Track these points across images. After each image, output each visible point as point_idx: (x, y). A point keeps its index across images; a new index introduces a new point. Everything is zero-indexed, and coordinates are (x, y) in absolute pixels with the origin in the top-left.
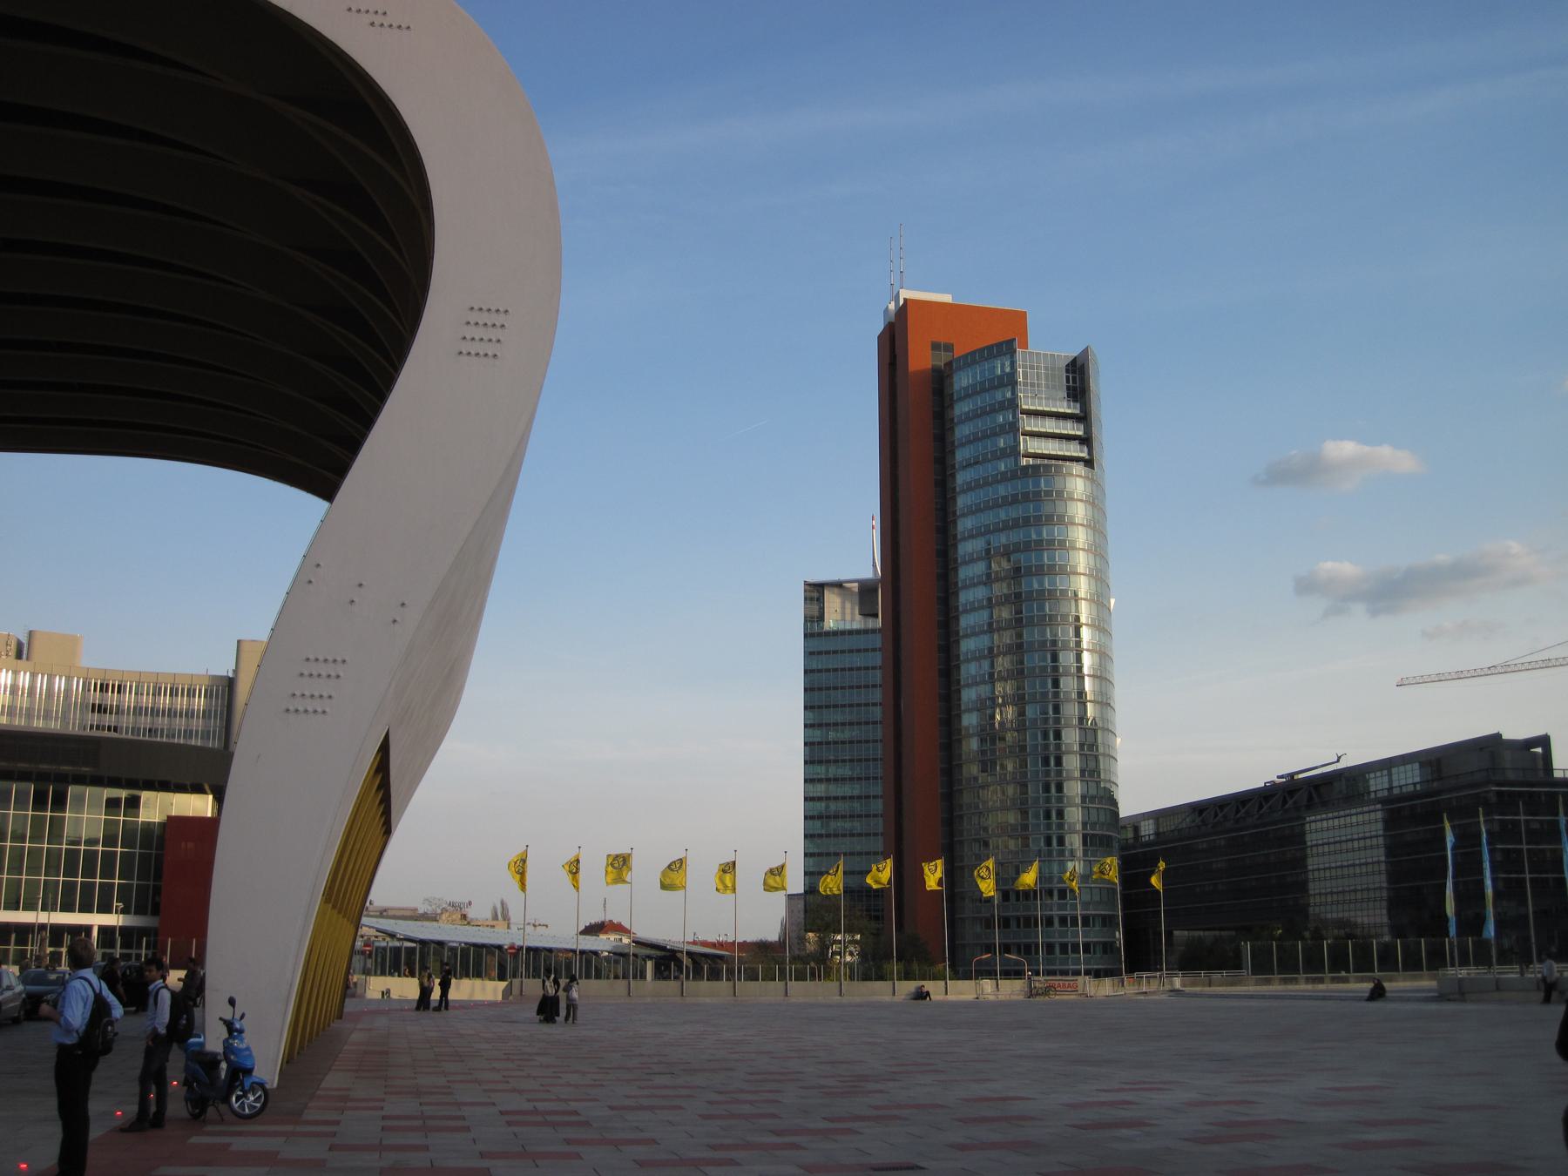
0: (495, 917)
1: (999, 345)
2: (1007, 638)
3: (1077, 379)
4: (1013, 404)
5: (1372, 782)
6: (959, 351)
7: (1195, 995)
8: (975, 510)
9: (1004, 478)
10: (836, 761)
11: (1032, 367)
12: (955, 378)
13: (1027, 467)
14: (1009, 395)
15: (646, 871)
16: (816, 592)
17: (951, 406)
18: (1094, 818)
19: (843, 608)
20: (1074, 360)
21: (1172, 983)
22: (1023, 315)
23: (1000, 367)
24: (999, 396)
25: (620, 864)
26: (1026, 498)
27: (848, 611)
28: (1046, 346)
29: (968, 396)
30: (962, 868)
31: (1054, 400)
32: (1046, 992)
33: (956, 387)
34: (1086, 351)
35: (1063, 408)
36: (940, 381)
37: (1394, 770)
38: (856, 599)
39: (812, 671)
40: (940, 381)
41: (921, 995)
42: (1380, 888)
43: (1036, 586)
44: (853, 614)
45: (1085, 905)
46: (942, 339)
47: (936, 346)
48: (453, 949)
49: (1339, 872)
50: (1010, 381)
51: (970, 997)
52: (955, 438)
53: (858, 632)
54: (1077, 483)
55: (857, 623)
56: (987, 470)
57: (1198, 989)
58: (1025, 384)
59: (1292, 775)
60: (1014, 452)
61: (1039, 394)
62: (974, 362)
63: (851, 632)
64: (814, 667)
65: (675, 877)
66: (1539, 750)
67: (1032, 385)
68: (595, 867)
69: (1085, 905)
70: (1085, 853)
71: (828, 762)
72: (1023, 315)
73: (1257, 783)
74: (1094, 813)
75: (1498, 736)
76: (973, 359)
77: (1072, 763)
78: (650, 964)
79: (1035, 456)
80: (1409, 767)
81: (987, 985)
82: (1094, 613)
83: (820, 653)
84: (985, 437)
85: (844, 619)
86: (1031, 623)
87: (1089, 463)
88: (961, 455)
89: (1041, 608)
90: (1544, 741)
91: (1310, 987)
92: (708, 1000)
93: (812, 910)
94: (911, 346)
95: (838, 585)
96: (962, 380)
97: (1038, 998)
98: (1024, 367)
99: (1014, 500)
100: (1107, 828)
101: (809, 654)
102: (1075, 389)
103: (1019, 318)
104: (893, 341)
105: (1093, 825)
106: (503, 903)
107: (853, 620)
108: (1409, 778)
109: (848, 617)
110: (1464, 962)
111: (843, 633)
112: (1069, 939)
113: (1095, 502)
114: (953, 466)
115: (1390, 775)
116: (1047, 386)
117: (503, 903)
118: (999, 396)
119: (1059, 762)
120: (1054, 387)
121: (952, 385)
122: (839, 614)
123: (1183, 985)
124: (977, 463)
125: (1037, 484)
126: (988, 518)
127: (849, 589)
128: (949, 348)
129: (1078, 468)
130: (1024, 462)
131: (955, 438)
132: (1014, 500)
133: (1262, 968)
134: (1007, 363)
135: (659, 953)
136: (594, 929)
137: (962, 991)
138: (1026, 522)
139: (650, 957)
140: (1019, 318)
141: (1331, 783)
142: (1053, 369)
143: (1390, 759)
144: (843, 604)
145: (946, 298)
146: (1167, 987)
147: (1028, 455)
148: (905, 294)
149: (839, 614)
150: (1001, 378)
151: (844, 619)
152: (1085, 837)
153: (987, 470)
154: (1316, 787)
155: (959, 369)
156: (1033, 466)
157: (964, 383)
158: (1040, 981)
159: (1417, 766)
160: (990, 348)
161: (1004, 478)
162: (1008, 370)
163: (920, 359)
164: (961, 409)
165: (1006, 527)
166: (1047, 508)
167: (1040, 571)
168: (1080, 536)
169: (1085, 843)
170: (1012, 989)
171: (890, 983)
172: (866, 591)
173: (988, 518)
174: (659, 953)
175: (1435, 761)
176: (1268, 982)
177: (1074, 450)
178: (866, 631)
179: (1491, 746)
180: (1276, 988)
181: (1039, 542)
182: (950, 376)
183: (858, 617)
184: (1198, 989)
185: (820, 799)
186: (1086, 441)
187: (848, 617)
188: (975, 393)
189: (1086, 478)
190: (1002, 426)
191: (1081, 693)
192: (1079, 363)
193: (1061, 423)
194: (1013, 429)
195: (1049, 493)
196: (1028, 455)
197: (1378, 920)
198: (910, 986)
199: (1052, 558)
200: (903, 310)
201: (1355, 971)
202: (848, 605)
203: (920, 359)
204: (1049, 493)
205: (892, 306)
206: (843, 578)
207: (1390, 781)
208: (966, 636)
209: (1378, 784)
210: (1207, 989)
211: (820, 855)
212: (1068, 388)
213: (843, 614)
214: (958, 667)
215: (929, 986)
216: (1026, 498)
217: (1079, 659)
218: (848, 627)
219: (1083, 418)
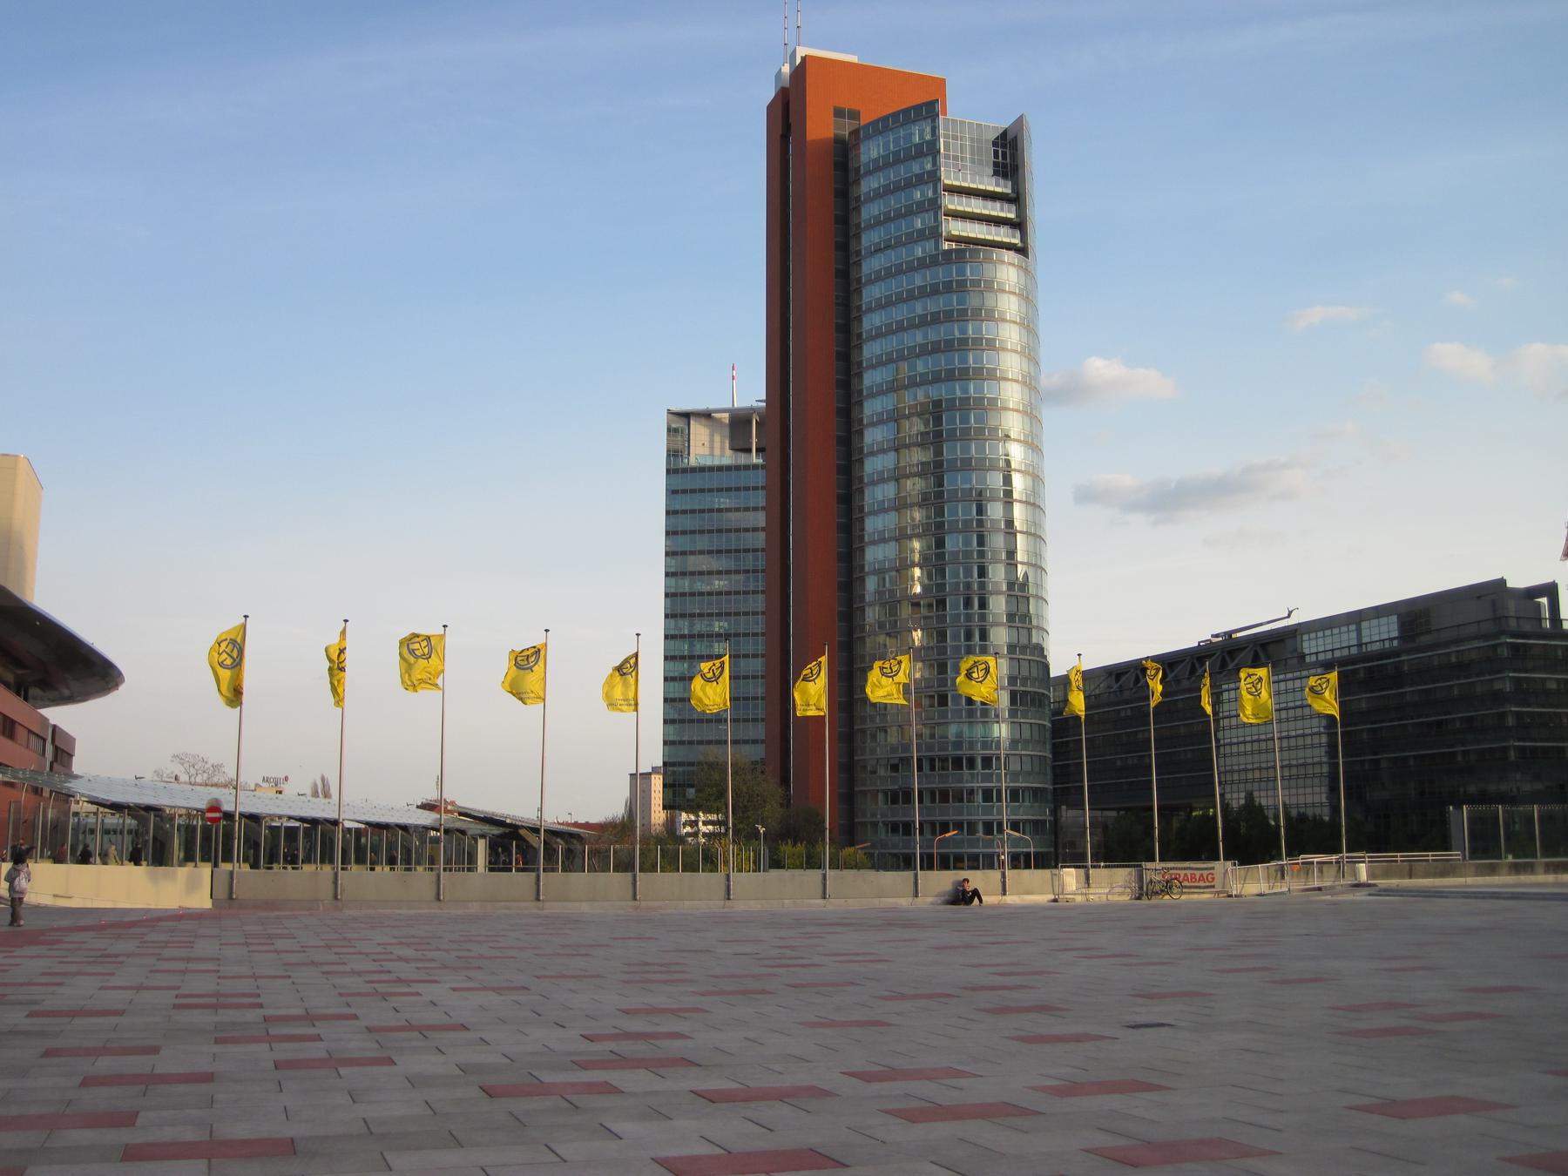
0: (315, 794)
1: (918, 108)
2: (917, 456)
3: (1008, 154)
4: (934, 177)
5: (1305, 644)
6: (865, 119)
7: (1387, 891)
8: (886, 304)
9: (922, 264)
10: (701, 615)
11: (955, 138)
12: (863, 148)
13: (950, 251)
14: (929, 167)
15: (475, 664)
16: (683, 418)
17: (857, 182)
18: (1025, 672)
19: (712, 441)
20: (1004, 134)
21: (1355, 874)
22: (942, 82)
23: (918, 133)
24: (916, 168)
25: (419, 655)
26: (948, 288)
27: (717, 445)
28: (972, 111)
29: (878, 169)
30: (863, 731)
31: (981, 176)
32: (1167, 888)
33: (864, 159)
34: (1020, 121)
35: (991, 185)
36: (843, 155)
37: (1365, 624)
38: (727, 431)
39: (676, 512)
40: (843, 155)
41: (963, 897)
42: (1321, 763)
43: (958, 393)
44: (722, 449)
45: (1014, 776)
46: (847, 105)
47: (839, 113)
48: (274, 830)
49: (1300, 741)
50: (930, 149)
51: (1044, 898)
52: (862, 228)
53: (729, 468)
54: (1007, 271)
55: (729, 458)
56: (900, 256)
57: (1394, 882)
58: (947, 157)
59: (1229, 634)
60: (935, 233)
61: (964, 168)
62: (886, 129)
63: (720, 468)
64: (678, 507)
65: (531, 680)
66: (1544, 600)
67: (956, 158)
68: (372, 662)
69: (1014, 776)
70: (1013, 713)
71: (692, 615)
72: (942, 82)
73: (595, 819)
74: (1025, 665)
75: (1502, 582)
76: (883, 125)
77: (999, 605)
78: (482, 845)
79: (959, 240)
80: (1384, 620)
81: (1070, 877)
82: (1028, 427)
83: (684, 492)
84: (899, 216)
85: (712, 454)
86: (952, 436)
87: (1022, 250)
88: (869, 239)
89: (965, 420)
90: (1551, 590)
91: (1551, 878)
92: (585, 907)
93: (686, 780)
94: (811, 111)
95: (706, 415)
96: (871, 151)
97: (1155, 900)
98: (946, 136)
99: (934, 291)
100: (1034, 688)
101: (672, 492)
102: (1004, 165)
103: (941, 83)
104: (786, 113)
105: (1024, 681)
106: (323, 779)
107: (722, 455)
108: (1384, 633)
109: (717, 452)
110: (1054, 851)
111: (711, 469)
112: (994, 817)
113: (1027, 297)
114: (858, 253)
115: (1359, 631)
116: (973, 161)
117: (323, 779)
118: (916, 168)
119: (983, 604)
120: (980, 162)
121: (858, 156)
122: (706, 448)
123: (1371, 875)
124: (888, 247)
125: (962, 272)
126: (899, 313)
127: (719, 421)
128: (854, 115)
129: (1009, 256)
130: (946, 246)
131: (862, 228)
132: (934, 291)
133: (1484, 847)
134: (928, 129)
135: (496, 831)
136: (428, 807)
137: (1030, 890)
138: (948, 317)
139: (483, 836)
140: (941, 83)
141: (1282, 641)
142: (979, 141)
143: (1360, 612)
144: (712, 436)
145: (854, 59)
146: (1349, 881)
147: (950, 239)
148: (802, 52)
149: (706, 448)
150: (919, 147)
151: (712, 454)
152: (1013, 695)
153: (900, 256)
154: (1264, 646)
155: (868, 137)
156: (956, 250)
157: (874, 154)
158: (1155, 869)
159: (1394, 618)
160: (906, 111)
161: (922, 264)
162: (928, 137)
163: (820, 126)
164: (869, 185)
165: (923, 322)
166: (973, 301)
167: (964, 375)
168: (1010, 335)
169: (1013, 700)
170: (1108, 886)
171: (909, 874)
172: (739, 423)
173: (899, 313)
174: (496, 831)
175: (1415, 616)
176: (1493, 870)
177: (1002, 235)
178: (738, 468)
179: (1495, 590)
180: (1503, 880)
181: (964, 341)
182: (857, 146)
183: (728, 452)
184: (1394, 882)
185: (683, 658)
186: (1019, 225)
187: (717, 452)
188: (887, 165)
189: (1019, 267)
190: (920, 204)
191: (1010, 523)
192: (1009, 137)
193: (990, 204)
194: (934, 205)
195: (976, 283)
196: (950, 239)
197: (1317, 799)
198: (942, 881)
199: (978, 360)
200: (801, 71)
201: (1543, 856)
202: (717, 438)
203: (820, 126)
204: (976, 283)
205: (786, 69)
206: (712, 406)
207: (1359, 636)
208: (872, 454)
209: (1310, 646)
210: (1407, 882)
211: (682, 721)
212: (996, 164)
213: (712, 448)
214: (862, 491)
215: (977, 879)
216: (948, 288)
217: (1008, 480)
218: (717, 462)
219: (1016, 198)
